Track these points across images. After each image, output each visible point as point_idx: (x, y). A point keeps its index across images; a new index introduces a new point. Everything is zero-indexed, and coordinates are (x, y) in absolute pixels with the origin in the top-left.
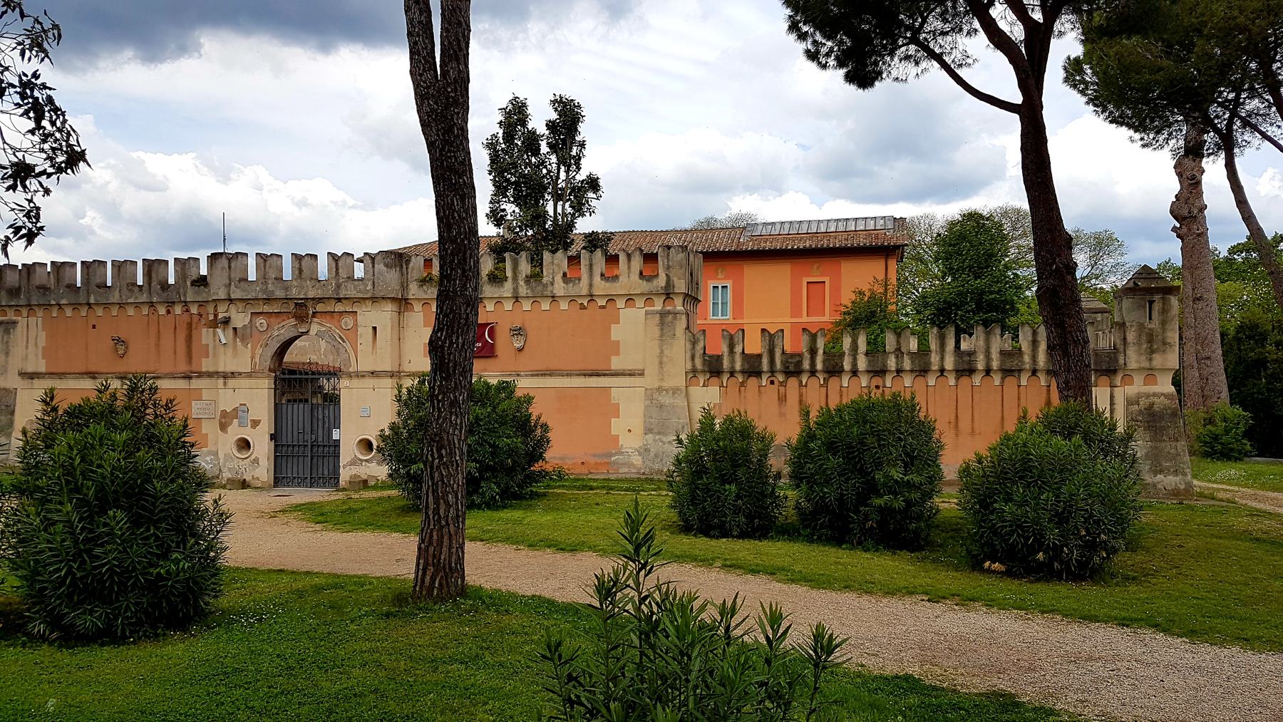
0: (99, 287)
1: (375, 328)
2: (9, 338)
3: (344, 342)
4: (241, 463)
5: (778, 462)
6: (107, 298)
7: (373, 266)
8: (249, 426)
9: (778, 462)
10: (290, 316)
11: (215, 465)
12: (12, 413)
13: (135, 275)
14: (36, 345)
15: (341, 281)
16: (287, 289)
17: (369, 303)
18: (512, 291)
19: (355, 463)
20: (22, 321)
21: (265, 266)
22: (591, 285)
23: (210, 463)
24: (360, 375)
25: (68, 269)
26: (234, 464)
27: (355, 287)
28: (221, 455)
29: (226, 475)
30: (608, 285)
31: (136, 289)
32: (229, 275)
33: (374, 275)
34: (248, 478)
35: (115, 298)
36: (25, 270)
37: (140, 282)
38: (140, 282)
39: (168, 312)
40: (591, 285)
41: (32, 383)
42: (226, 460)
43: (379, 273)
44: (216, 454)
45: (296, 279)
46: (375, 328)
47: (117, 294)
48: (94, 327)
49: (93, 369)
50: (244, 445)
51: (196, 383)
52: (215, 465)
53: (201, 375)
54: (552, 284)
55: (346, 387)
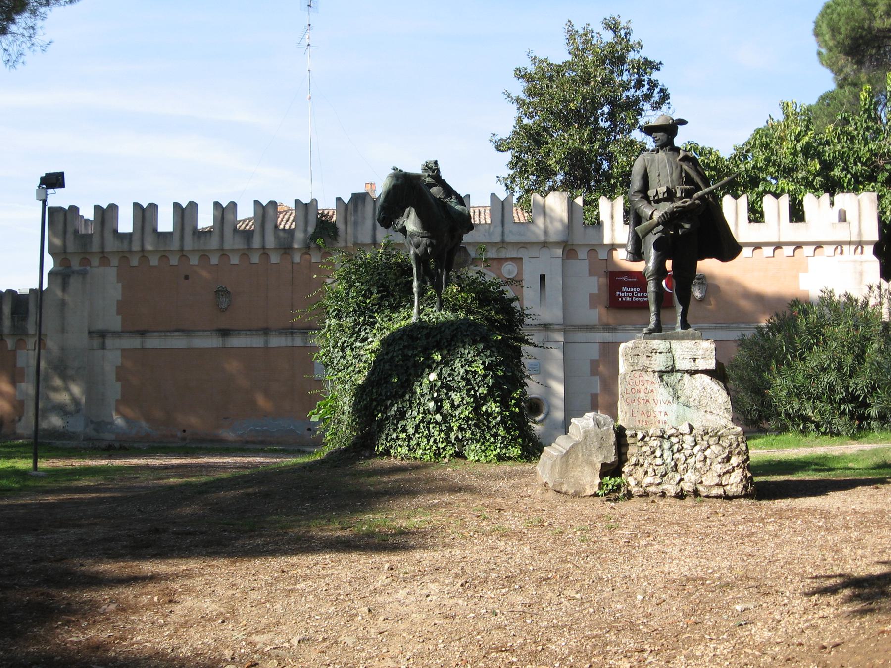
1: (543, 277)
46: (543, 277)
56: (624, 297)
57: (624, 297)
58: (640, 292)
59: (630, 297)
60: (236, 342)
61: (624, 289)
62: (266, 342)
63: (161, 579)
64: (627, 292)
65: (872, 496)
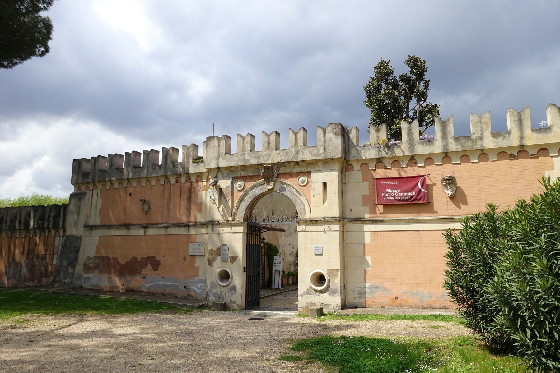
0: (134, 167)
1: (325, 184)
2: (81, 203)
3: (300, 194)
4: (223, 290)
5: (283, 193)
6: (139, 175)
7: (325, 135)
8: (229, 261)
9: (283, 193)
10: (260, 178)
11: (203, 290)
12: (78, 252)
13: (158, 160)
14: (96, 207)
15: (299, 148)
16: (258, 157)
17: (320, 164)
18: (442, 148)
19: (308, 293)
20: (89, 193)
21: (243, 143)
22: (522, 138)
23: (200, 289)
24: (314, 222)
25: (118, 158)
26: (218, 290)
27: (310, 152)
28: (208, 283)
29: (212, 298)
30: (540, 135)
31: (157, 168)
32: (219, 151)
33: (325, 142)
34: (227, 300)
35: (144, 174)
36: (93, 161)
37: (160, 163)
38: (160, 163)
39: (177, 182)
40: (522, 138)
41: (92, 232)
42: (212, 288)
43: (330, 140)
44: (204, 282)
45: (265, 150)
46: (325, 184)
47: (145, 172)
48: (130, 194)
49: (128, 222)
50: (225, 276)
51: (192, 231)
52: (203, 290)
53: (196, 224)
54: (481, 139)
55: (303, 231)
56: (388, 196)
57: (388, 196)
58: (401, 192)
59: (392, 197)
60: (151, 232)
61: (388, 190)
62: (145, 233)
63: (522, 136)
64: (390, 193)
65: (393, 69)
